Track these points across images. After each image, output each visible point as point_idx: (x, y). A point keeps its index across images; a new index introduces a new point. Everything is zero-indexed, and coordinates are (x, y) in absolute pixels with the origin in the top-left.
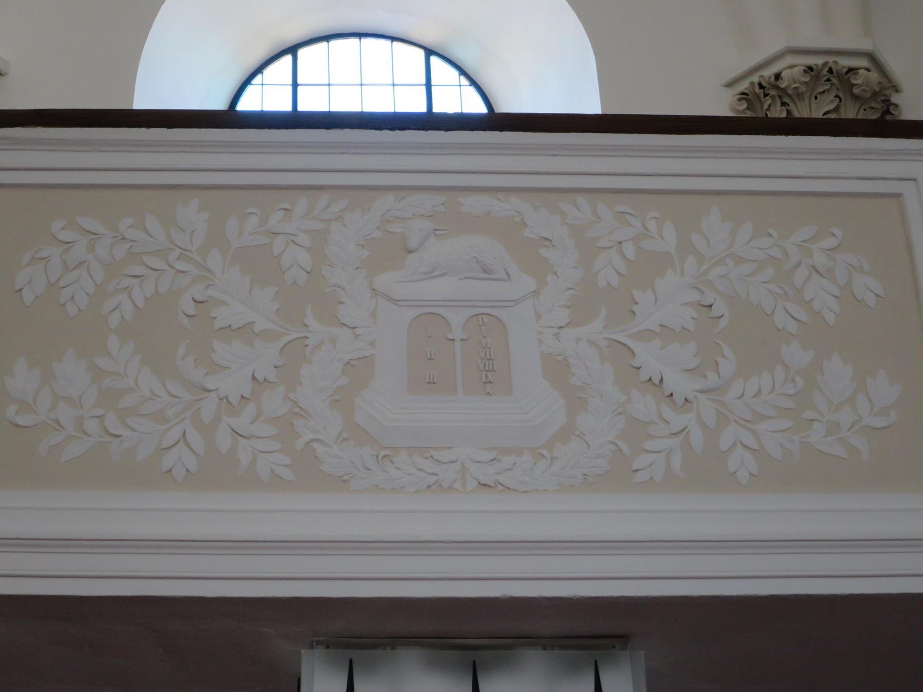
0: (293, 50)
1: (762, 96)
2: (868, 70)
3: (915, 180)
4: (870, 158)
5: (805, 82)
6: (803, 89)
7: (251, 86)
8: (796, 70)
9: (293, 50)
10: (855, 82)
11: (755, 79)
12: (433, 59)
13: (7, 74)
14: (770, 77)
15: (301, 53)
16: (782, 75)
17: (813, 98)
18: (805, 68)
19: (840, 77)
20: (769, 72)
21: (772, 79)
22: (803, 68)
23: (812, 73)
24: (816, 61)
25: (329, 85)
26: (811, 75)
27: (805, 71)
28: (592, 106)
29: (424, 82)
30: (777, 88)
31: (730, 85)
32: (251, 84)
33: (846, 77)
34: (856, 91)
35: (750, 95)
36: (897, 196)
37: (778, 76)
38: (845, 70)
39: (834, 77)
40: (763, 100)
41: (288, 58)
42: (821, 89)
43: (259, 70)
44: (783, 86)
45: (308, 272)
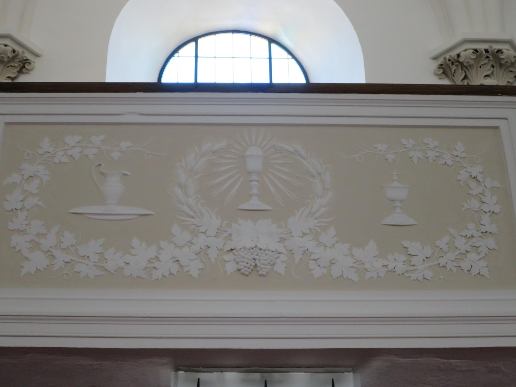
0: (195, 39)
1: (451, 65)
2: (508, 50)
3: (506, 119)
4: (158, 323)
5: (474, 59)
6: (472, 62)
7: (174, 57)
8: (468, 51)
9: (195, 39)
10: (501, 57)
11: (448, 57)
12: (273, 45)
13: (42, 56)
14: (455, 56)
15: (200, 41)
16: (461, 54)
17: (479, 67)
18: (472, 51)
19: (493, 54)
20: (454, 53)
21: (456, 57)
22: (472, 51)
23: (478, 54)
24: (482, 47)
25: (215, 57)
26: (477, 55)
27: (473, 53)
28: (360, 79)
29: (268, 57)
30: (459, 62)
31: (435, 58)
32: (174, 57)
33: (497, 54)
34: (503, 62)
35: (444, 65)
36: (496, 128)
37: (458, 55)
38: (496, 51)
39: (489, 54)
40: (451, 67)
41: (193, 44)
42: (483, 63)
43: (176, 51)
44: (461, 61)
45: (487, 267)
